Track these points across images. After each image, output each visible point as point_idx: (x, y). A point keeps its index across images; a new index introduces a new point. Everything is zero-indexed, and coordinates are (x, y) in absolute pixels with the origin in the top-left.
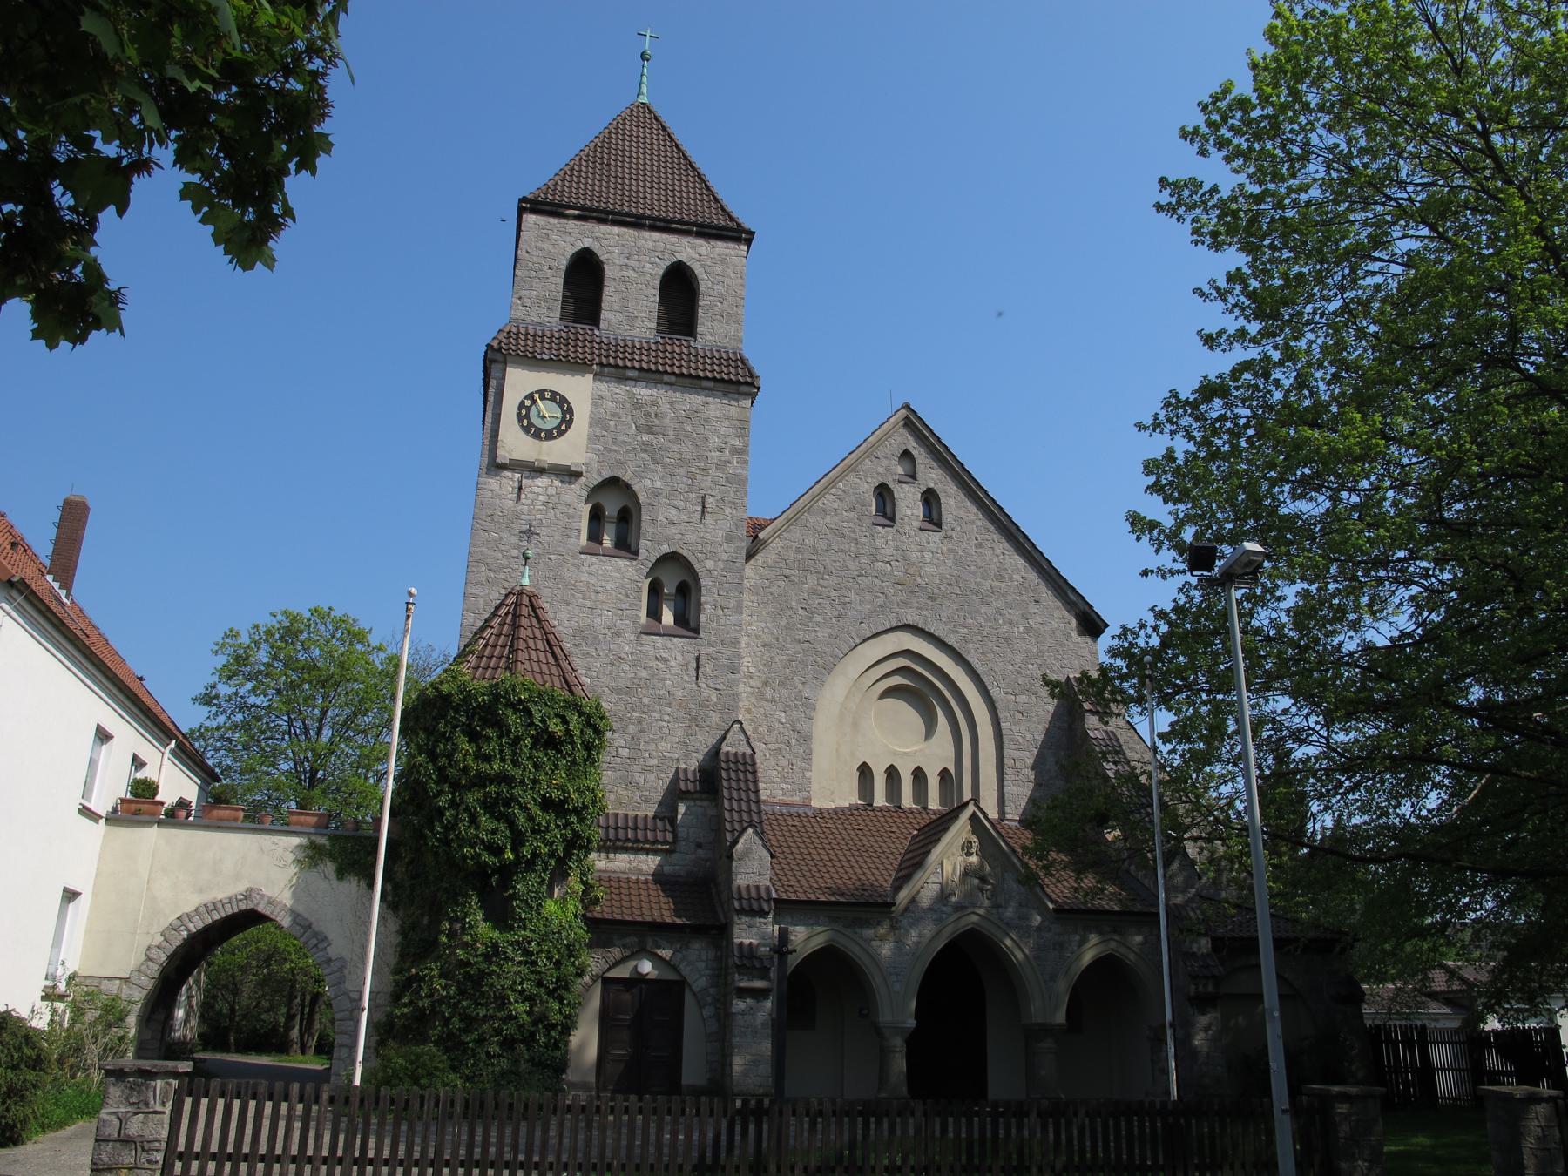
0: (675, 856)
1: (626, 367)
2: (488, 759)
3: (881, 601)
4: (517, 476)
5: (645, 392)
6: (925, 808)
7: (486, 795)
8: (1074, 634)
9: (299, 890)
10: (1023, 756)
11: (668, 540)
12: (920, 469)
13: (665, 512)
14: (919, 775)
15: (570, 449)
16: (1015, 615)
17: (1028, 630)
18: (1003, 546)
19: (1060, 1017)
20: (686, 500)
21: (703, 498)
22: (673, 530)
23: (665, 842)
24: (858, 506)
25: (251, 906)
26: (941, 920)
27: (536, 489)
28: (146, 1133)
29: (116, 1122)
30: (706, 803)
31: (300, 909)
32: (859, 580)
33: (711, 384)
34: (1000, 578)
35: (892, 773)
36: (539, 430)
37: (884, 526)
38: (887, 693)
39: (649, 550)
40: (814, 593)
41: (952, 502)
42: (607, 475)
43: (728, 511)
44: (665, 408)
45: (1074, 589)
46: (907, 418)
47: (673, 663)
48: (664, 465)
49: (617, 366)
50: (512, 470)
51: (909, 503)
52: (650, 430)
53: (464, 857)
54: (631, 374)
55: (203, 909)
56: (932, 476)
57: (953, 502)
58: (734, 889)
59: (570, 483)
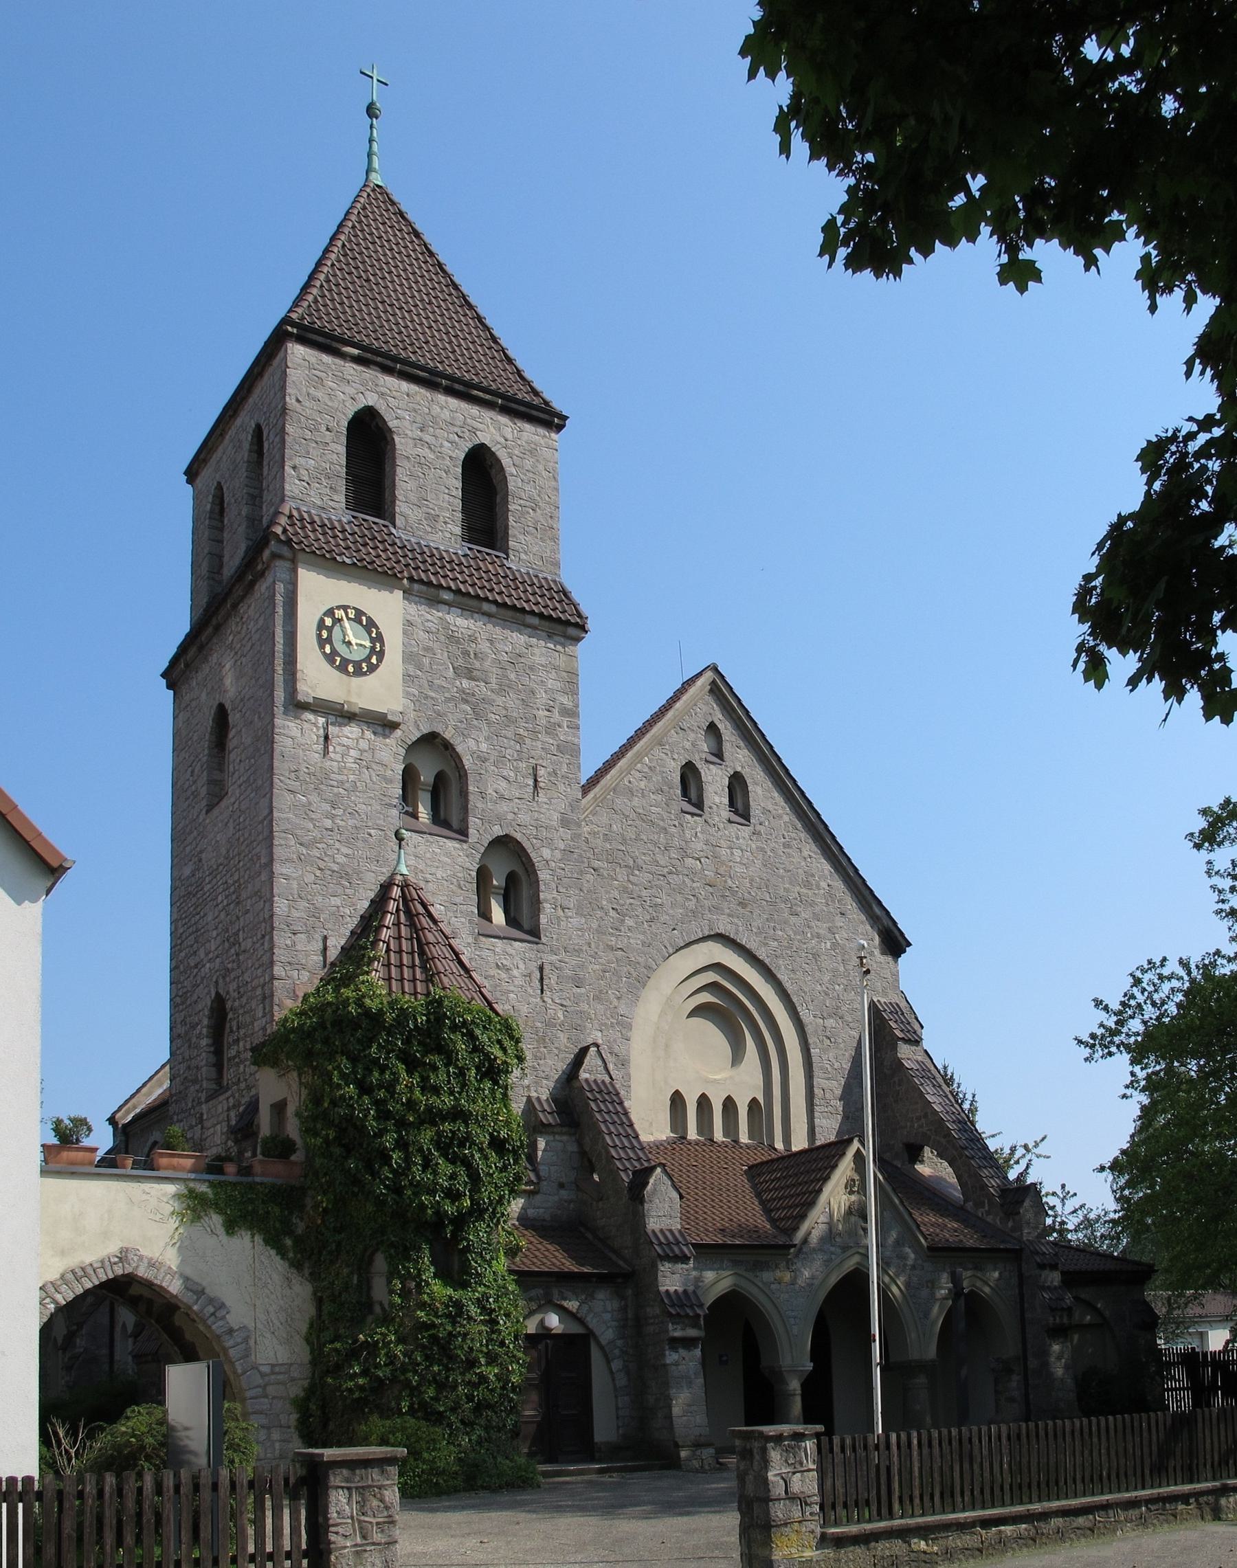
0: (538, 1197)
1: (441, 586)
2: (436, 1090)
3: (692, 904)
4: (321, 720)
5: (461, 622)
7: (439, 1134)
8: (877, 952)
9: (185, 1248)
11: (500, 819)
12: (727, 748)
15: (382, 691)
17: (835, 945)
18: (810, 848)
19: (932, 1352)
21: (535, 769)
22: (504, 807)
25: (129, 1270)
27: (345, 741)
28: (805, 1489)
29: (782, 1482)
30: (565, 1138)
31: (189, 1272)
32: (670, 877)
34: (807, 884)
35: (704, 1103)
36: (345, 662)
37: (693, 815)
38: (691, 1015)
39: (481, 832)
40: (625, 890)
41: (759, 790)
42: (425, 730)
43: (562, 788)
44: (484, 646)
45: (879, 903)
46: (714, 682)
47: (515, 972)
48: (489, 723)
49: (430, 584)
50: (314, 712)
52: (470, 674)
53: (422, 1207)
54: (446, 596)
55: (70, 1276)
56: (739, 757)
57: (761, 791)
58: (650, 1232)
59: (385, 736)
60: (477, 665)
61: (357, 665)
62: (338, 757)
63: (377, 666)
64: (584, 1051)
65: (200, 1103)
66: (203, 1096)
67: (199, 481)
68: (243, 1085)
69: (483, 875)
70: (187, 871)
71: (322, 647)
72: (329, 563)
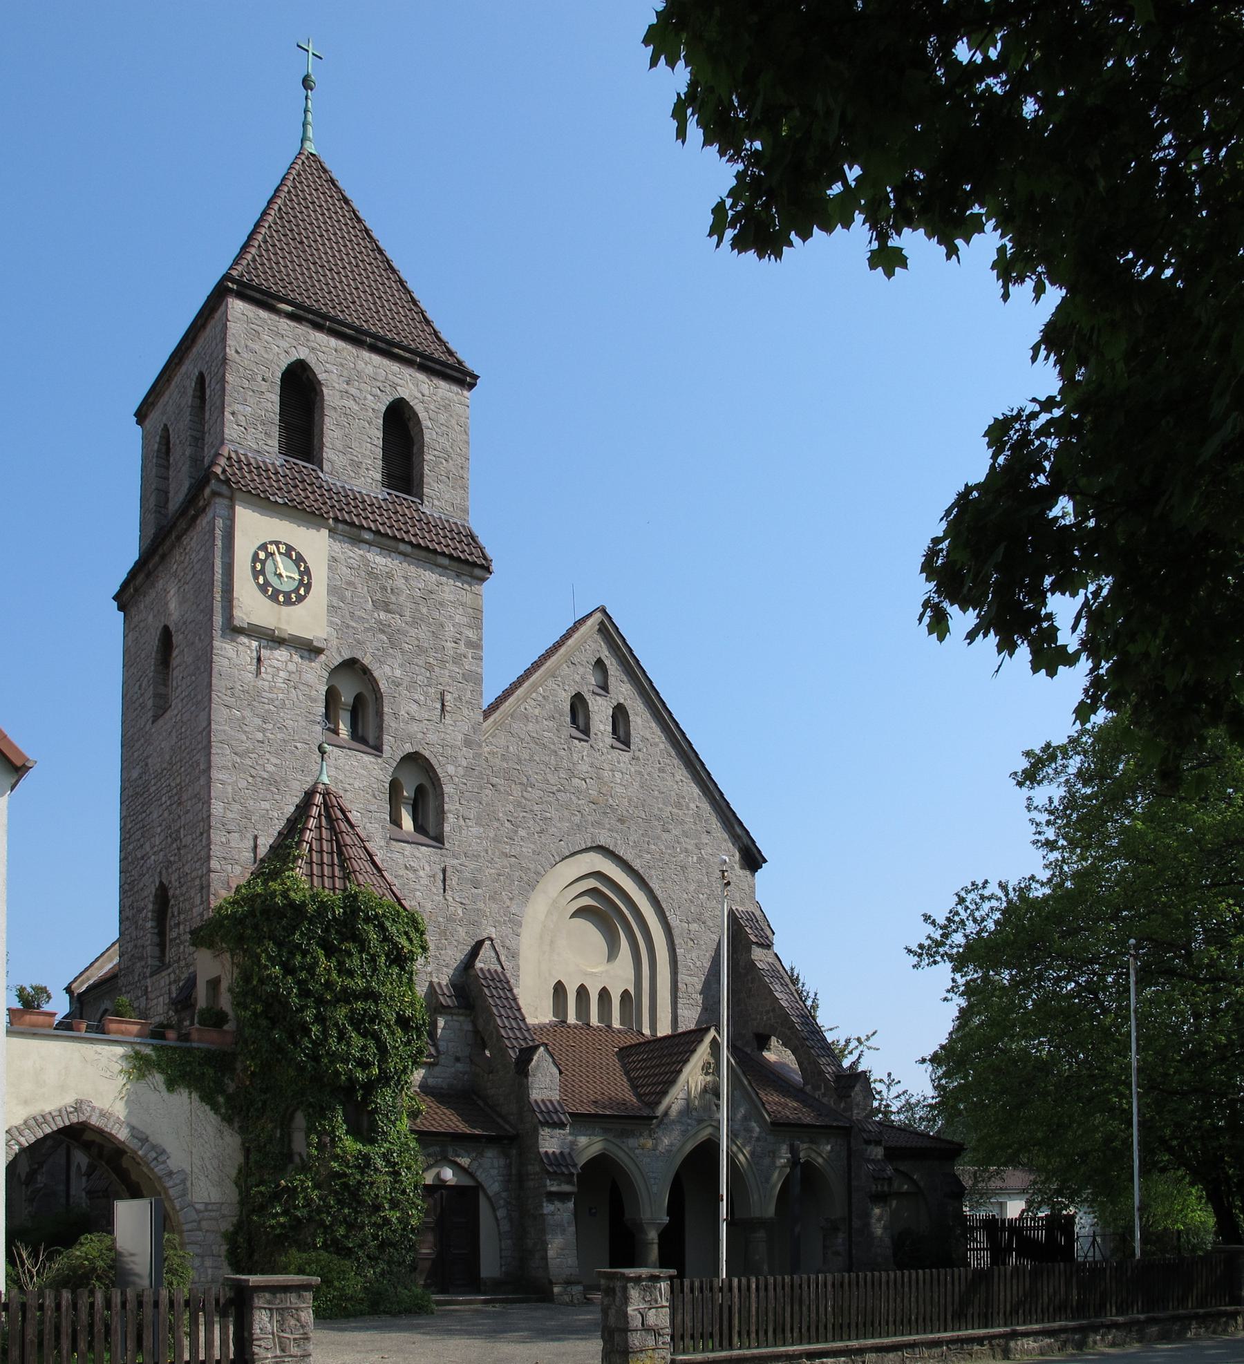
0: (437, 1069)
2: (351, 974)
3: (577, 819)
4: (255, 644)
5: (379, 559)
6: (609, 1026)
7: (352, 1011)
8: (737, 867)
10: (693, 982)
11: (411, 737)
13: (407, 707)
14: (604, 994)
15: (309, 619)
16: (690, 844)
17: (700, 860)
18: (682, 773)
19: (770, 1211)
20: (426, 694)
21: (442, 694)
22: (415, 727)
23: (430, 1056)
24: (557, 715)
26: (686, 1131)
27: (275, 663)
28: (659, 1323)
30: (461, 1018)
31: (135, 1122)
32: (559, 795)
33: (446, 562)
34: (678, 805)
35: (582, 992)
36: (277, 592)
37: (580, 740)
39: (394, 749)
41: (639, 720)
42: (347, 655)
43: (466, 712)
44: (400, 583)
45: (741, 824)
46: (602, 623)
47: (421, 873)
48: (403, 652)
50: (249, 636)
51: (601, 720)
54: (367, 536)
55: (32, 1122)
56: (623, 691)
57: (641, 722)
59: (311, 660)
60: (393, 599)
61: (287, 595)
62: (269, 677)
63: (305, 597)
64: (480, 944)
65: (145, 978)
66: (148, 971)
67: (147, 422)
68: (183, 963)
69: (395, 787)
70: (135, 775)
71: (256, 578)
72: (264, 503)
